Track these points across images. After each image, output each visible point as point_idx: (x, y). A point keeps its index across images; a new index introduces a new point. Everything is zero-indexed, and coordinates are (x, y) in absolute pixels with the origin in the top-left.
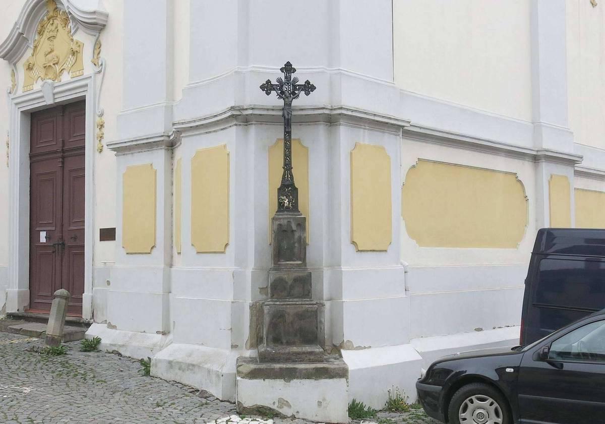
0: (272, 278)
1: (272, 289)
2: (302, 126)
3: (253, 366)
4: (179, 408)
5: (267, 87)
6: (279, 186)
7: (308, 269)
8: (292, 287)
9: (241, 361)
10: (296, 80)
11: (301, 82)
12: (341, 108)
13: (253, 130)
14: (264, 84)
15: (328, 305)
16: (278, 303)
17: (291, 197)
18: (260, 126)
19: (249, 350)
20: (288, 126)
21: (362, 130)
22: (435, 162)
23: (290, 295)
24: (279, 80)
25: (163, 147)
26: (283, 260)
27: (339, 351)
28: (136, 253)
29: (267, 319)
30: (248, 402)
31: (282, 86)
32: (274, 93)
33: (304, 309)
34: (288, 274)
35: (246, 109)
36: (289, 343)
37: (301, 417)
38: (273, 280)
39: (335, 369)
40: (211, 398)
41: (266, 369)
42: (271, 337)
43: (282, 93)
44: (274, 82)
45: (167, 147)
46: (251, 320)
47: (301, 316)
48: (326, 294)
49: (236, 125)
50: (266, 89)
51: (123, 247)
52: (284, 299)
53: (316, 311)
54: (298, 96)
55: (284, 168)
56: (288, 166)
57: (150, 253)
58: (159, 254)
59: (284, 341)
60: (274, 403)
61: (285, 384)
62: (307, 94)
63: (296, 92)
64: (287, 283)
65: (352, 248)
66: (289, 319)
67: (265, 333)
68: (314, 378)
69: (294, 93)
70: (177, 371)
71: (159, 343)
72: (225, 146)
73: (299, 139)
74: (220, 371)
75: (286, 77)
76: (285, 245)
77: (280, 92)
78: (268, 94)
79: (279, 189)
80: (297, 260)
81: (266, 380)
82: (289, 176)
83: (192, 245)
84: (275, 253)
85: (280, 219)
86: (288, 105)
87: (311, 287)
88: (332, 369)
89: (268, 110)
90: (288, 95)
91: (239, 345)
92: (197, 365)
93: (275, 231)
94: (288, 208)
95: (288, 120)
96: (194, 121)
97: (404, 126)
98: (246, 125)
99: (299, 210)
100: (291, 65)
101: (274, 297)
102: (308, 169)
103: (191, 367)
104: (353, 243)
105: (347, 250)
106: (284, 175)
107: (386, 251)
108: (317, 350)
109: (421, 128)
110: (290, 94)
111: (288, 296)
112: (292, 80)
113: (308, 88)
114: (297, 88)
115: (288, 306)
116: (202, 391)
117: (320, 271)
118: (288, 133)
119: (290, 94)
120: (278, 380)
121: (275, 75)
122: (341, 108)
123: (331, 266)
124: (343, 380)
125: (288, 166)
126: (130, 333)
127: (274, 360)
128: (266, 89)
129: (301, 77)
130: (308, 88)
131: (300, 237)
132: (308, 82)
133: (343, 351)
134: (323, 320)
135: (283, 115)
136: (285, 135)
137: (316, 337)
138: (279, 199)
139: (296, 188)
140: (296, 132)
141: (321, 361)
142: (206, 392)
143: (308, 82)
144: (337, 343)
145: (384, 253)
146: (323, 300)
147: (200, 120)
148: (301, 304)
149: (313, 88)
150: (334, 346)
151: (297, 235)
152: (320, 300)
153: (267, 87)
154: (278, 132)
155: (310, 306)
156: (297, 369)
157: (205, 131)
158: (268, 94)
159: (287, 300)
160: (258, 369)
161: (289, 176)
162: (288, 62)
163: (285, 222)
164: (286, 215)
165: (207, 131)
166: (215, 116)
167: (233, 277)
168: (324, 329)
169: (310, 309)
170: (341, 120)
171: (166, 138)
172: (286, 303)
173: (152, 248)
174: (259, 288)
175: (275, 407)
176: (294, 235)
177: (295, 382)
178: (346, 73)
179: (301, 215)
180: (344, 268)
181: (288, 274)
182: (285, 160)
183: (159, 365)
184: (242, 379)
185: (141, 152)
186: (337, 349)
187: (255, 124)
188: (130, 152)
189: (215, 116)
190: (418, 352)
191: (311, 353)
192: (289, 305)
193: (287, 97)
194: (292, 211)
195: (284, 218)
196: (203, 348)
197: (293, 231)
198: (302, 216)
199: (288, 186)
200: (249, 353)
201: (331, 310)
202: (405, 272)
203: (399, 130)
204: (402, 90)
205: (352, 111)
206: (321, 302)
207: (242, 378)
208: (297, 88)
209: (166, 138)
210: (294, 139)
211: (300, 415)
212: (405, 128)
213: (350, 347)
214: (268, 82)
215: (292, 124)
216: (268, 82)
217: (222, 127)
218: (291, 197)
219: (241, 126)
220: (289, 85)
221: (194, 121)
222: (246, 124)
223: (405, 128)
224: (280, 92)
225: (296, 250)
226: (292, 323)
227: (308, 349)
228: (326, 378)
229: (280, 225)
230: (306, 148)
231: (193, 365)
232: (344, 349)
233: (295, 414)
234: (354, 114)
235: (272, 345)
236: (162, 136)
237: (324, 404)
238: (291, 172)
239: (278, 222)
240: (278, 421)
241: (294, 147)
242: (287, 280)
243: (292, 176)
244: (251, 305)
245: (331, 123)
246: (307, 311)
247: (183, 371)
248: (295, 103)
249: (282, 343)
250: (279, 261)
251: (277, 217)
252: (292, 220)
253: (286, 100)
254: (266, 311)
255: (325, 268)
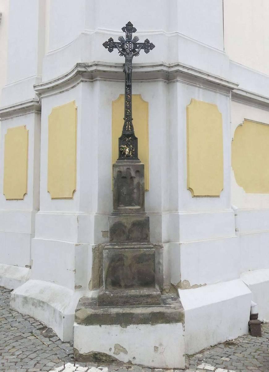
0: (111, 223)
1: (111, 233)
2: (142, 83)
3: (90, 311)
4: (17, 353)
5: (110, 45)
6: (120, 135)
7: (146, 213)
8: (130, 231)
9: (84, 303)
10: (136, 39)
11: (141, 41)
12: (178, 65)
13: (98, 85)
14: (106, 42)
15: (166, 247)
16: (117, 247)
17: (131, 146)
18: (104, 82)
19: (91, 290)
20: (129, 80)
21: (197, 88)
22: (257, 123)
23: (129, 239)
24: (121, 39)
25: (34, 111)
26: (122, 205)
27: (177, 291)
28: (12, 199)
29: (106, 263)
30: (84, 349)
31: (123, 44)
32: (116, 50)
33: (142, 252)
34: (127, 219)
35: (91, 66)
36: (127, 287)
37: (138, 363)
38: (112, 224)
39: (171, 313)
40: (53, 339)
41: (102, 314)
42: (109, 280)
43: (124, 50)
44: (116, 40)
45: (37, 111)
46: (94, 262)
47: (140, 259)
48: (164, 236)
49: (82, 81)
50: (108, 47)
51: (4, 195)
52: (123, 242)
53: (154, 255)
54: (138, 53)
55: (124, 119)
56: (128, 118)
57: (22, 199)
58: (29, 199)
59: (123, 284)
60: (110, 349)
61: (122, 330)
62: (147, 52)
63: (137, 50)
64: (126, 227)
65: (188, 193)
66: (127, 262)
67: (104, 276)
68: (151, 323)
69: (134, 50)
70: (31, 306)
71: (26, 276)
72: (74, 102)
73: (140, 95)
74: (62, 312)
75: (127, 36)
76: (124, 190)
77: (121, 49)
78: (110, 51)
79: (120, 139)
80: (136, 205)
81: (103, 326)
82: (130, 127)
83: (48, 192)
84: (115, 198)
85: (120, 166)
86: (129, 61)
87: (149, 231)
88: (168, 313)
89: (111, 66)
90: (128, 51)
91: (83, 287)
92: (46, 303)
93: (115, 178)
94: (128, 157)
95: (128, 75)
96: (51, 83)
97: (233, 89)
98: (92, 82)
99: (139, 158)
100: (132, 25)
101: (114, 241)
102: (148, 120)
103: (41, 304)
104: (190, 189)
105: (183, 195)
106: (125, 126)
107: (218, 196)
108: (155, 293)
109: (247, 92)
110: (131, 51)
111: (127, 240)
112: (132, 39)
113: (148, 46)
114: (138, 46)
115: (127, 250)
116: (49, 329)
117: (159, 215)
118: (128, 87)
119: (131, 51)
120: (114, 325)
121: (118, 34)
122: (178, 65)
123: (170, 210)
124: (180, 324)
125: (128, 118)
126: (6, 266)
127: (112, 303)
128: (108, 47)
129: (141, 36)
130: (148, 46)
131: (139, 184)
132: (147, 41)
133: (180, 291)
134: (161, 261)
135: (124, 71)
136: (126, 89)
137: (153, 277)
138: (120, 148)
139: (136, 137)
140: (135, 90)
141: (158, 304)
142: (50, 330)
143: (147, 41)
144: (175, 283)
145: (217, 199)
146: (161, 242)
147: (55, 81)
148: (140, 248)
149: (152, 46)
150: (172, 285)
151: (136, 181)
152: (158, 242)
153: (110, 45)
154: (121, 89)
155: (147, 250)
156: (133, 314)
157: (59, 91)
158: (110, 51)
159: (126, 244)
160: (94, 314)
161: (130, 127)
162: (129, 23)
163: (125, 168)
164: (126, 162)
165: (61, 91)
166: (66, 76)
167: (78, 221)
168: (162, 271)
169: (147, 253)
170: (178, 77)
171: (36, 104)
172: (125, 247)
173: (24, 195)
174: (102, 231)
175: (111, 353)
176: (133, 181)
177: (131, 328)
178: (183, 36)
179: (140, 162)
180: (181, 212)
181: (127, 219)
182: (126, 112)
183: (17, 300)
184: (78, 325)
185: (18, 116)
186: (175, 288)
187: (99, 80)
188: (10, 117)
189: (66, 76)
190: (247, 286)
191: (148, 296)
192: (127, 248)
193: (128, 54)
194: (132, 158)
195: (123, 166)
196: (53, 285)
197: (132, 178)
198: (141, 164)
199: (128, 136)
200: (92, 294)
201: (169, 252)
202: (236, 215)
203: (229, 92)
204: (231, 61)
205: (189, 69)
206: (160, 244)
207: (78, 323)
208: (138, 46)
209: (36, 104)
210: (135, 95)
211: (137, 361)
212: (234, 91)
213: (188, 286)
214: (111, 40)
215: (133, 81)
216: (111, 40)
217: (72, 86)
218: (131, 146)
219: (87, 83)
220: (130, 44)
221: (51, 83)
222: (91, 80)
223: (234, 91)
224: (121, 49)
225: (135, 196)
226: (130, 266)
227: (145, 291)
228: (162, 323)
229: (120, 172)
230: (147, 103)
231: (43, 303)
232: (181, 288)
233: (131, 360)
234: (190, 72)
235: (110, 288)
236: (32, 102)
237: (160, 349)
238: (131, 123)
239: (117, 169)
240: (114, 366)
241: (135, 103)
242: (125, 224)
243: (132, 126)
244: (94, 248)
245: (169, 80)
246: (145, 255)
247: (36, 307)
248: (136, 60)
249: (120, 286)
250: (118, 206)
251: (117, 164)
252: (131, 167)
253: (127, 56)
254: (105, 255)
255: (163, 213)
